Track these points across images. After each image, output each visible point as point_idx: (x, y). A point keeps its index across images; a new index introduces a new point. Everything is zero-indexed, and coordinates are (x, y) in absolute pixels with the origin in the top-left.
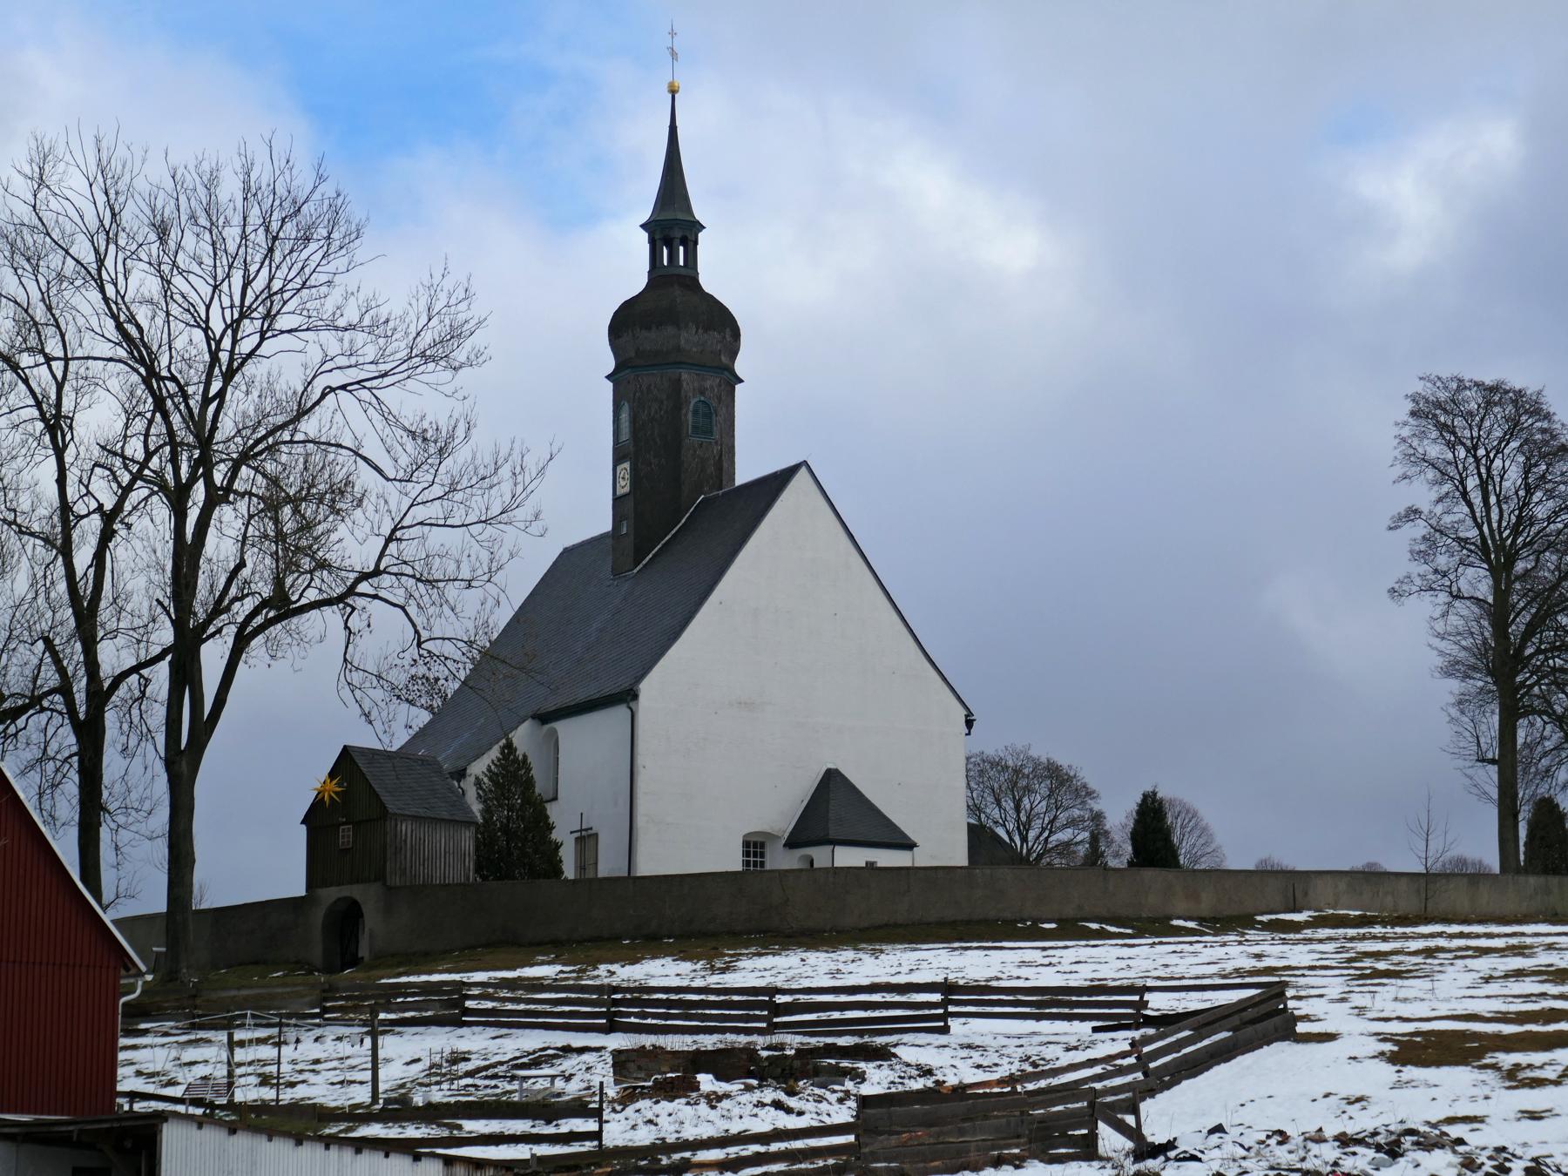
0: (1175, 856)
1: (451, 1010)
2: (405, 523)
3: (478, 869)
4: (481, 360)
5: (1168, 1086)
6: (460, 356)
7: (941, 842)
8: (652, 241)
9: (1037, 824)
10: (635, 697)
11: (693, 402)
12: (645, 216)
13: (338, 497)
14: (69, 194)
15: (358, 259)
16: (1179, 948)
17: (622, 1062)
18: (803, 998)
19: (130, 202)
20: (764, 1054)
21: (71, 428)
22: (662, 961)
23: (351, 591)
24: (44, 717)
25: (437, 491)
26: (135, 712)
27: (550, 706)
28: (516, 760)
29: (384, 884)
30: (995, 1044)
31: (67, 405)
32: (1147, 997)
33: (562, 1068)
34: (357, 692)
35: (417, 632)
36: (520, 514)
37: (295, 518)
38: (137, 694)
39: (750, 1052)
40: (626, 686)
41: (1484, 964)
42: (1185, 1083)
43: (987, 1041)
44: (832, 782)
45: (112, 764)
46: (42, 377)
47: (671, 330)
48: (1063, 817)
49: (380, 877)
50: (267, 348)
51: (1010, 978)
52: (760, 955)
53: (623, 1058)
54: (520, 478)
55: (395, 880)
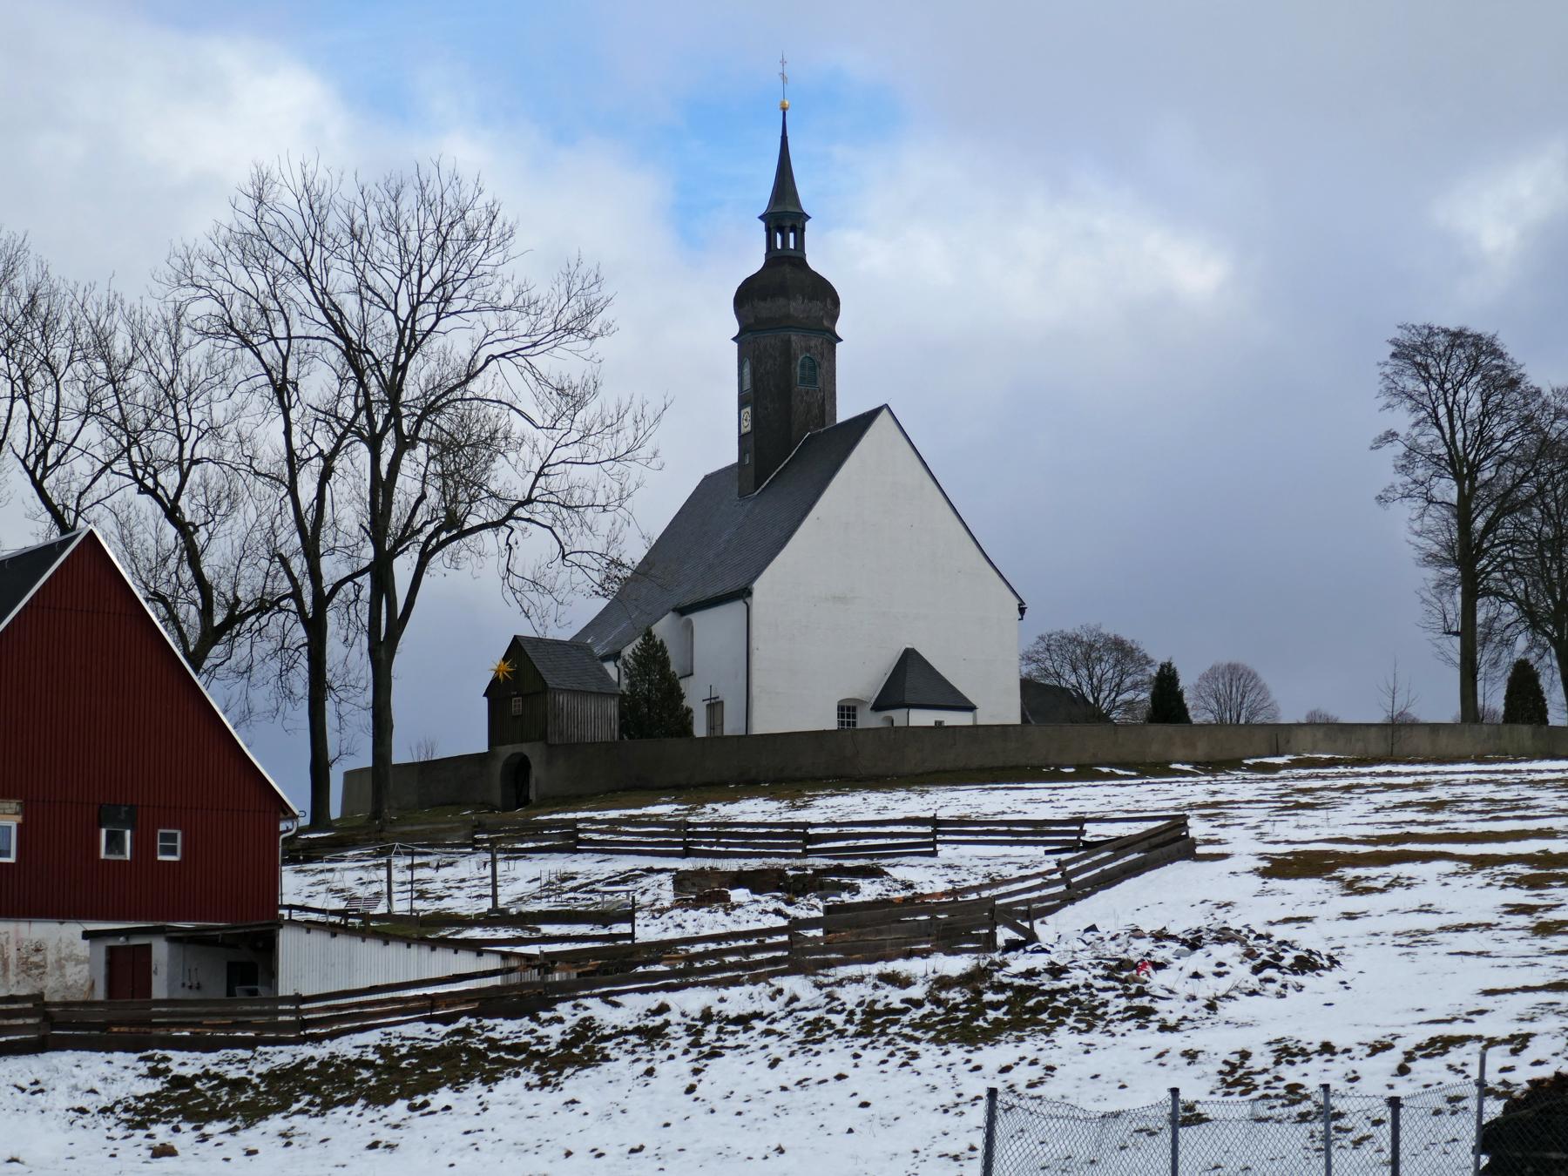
0: (1184, 711)
1: (571, 842)
2: (551, 461)
3: (622, 729)
5: (1086, 895)
6: (594, 328)
7: (999, 704)
8: (768, 230)
9: (1106, 687)
10: (750, 594)
12: (763, 209)
13: (490, 443)
14: (281, 208)
15: (512, 253)
16: (1155, 787)
17: (680, 880)
18: (846, 830)
19: (332, 213)
21: (296, 389)
23: (510, 516)
24: (282, 617)
25: (575, 436)
26: (352, 610)
27: (687, 601)
28: (655, 645)
31: (291, 375)
32: (1086, 826)
36: (642, 453)
37: (463, 458)
38: (352, 597)
39: (780, 873)
40: (743, 585)
41: (1381, 799)
42: (1100, 893)
43: (966, 863)
44: (910, 660)
45: (334, 648)
46: (269, 351)
47: (781, 301)
48: (1128, 681)
49: (543, 737)
50: (442, 326)
52: (832, 795)
55: (554, 739)
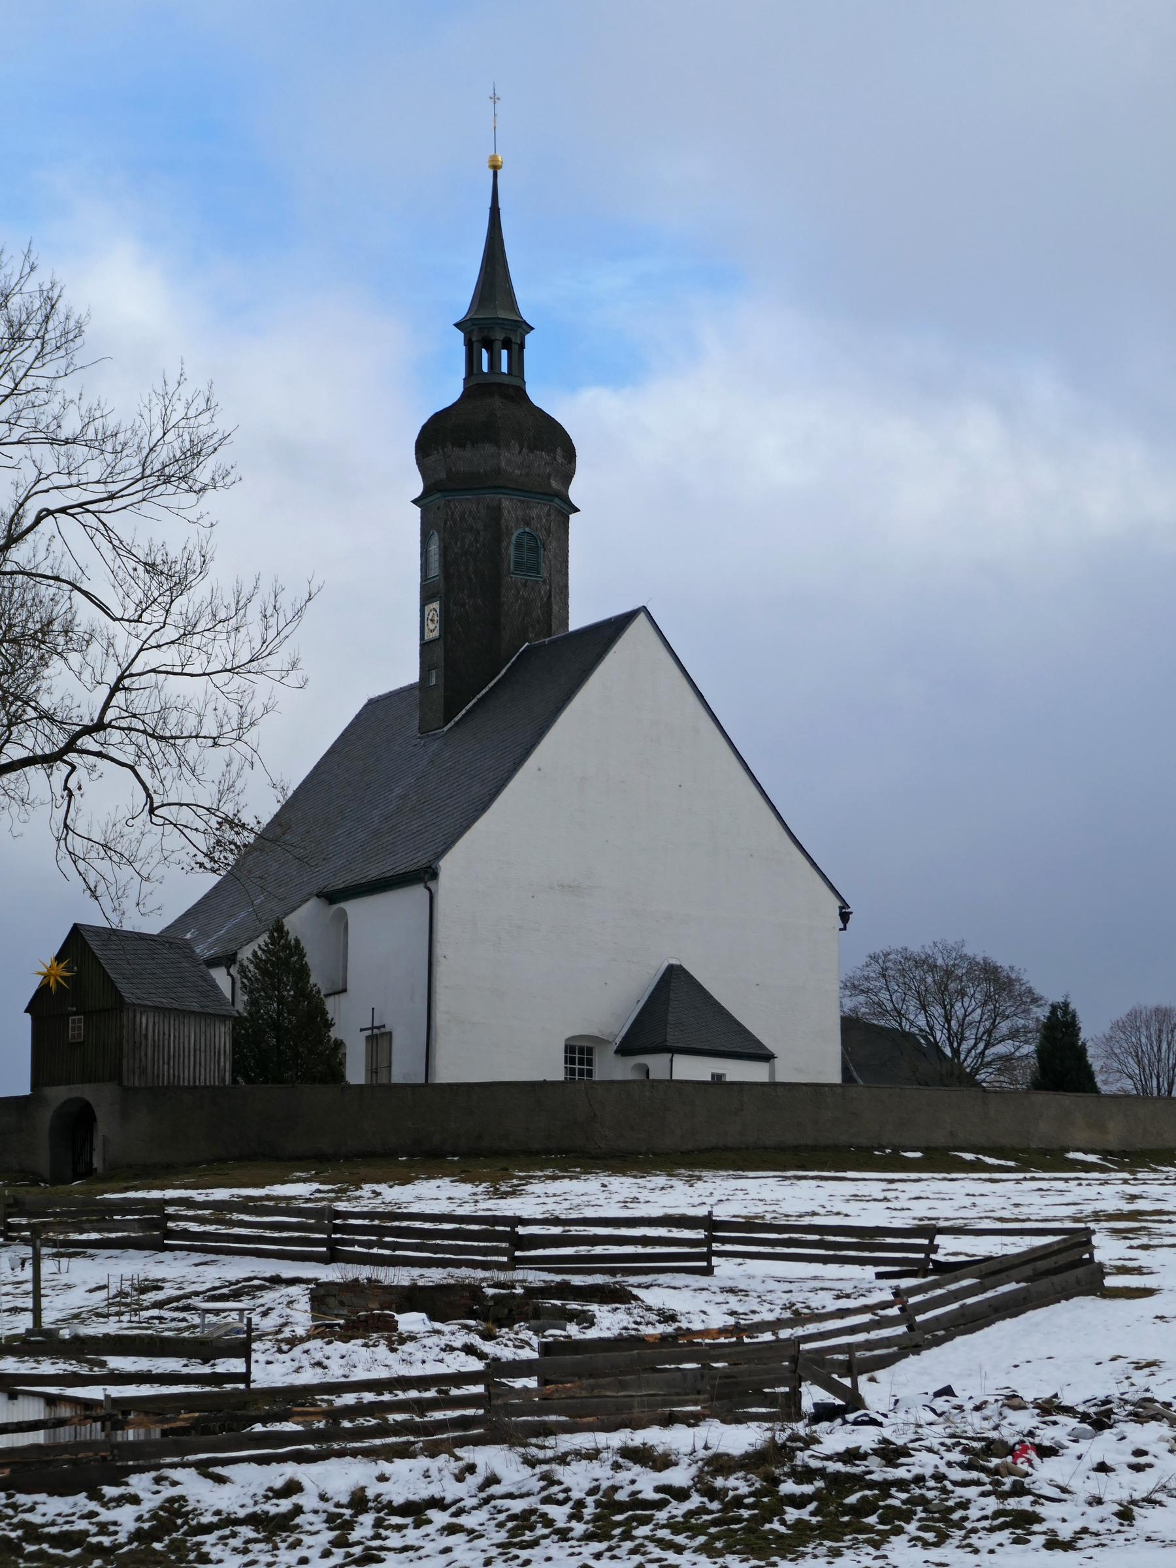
1: (156, 1234)
2: (135, 669)
3: (235, 1071)
4: (228, 480)
5: (938, 1342)
6: (203, 475)
7: (809, 1054)
8: (469, 343)
11: (516, 534)
12: (461, 313)
15: (78, 361)
18: (575, 1230)
20: (490, 1292)
22: (438, 1182)
23: (70, 747)
25: (171, 633)
27: (339, 884)
28: (287, 946)
29: (120, 1083)
30: (761, 1288)
32: (939, 1239)
33: (261, 1301)
34: (81, 864)
35: (149, 796)
36: (276, 662)
39: (475, 1291)
42: (959, 1340)
43: (755, 1286)
44: (675, 980)
47: (489, 449)
48: (1004, 1027)
49: (116, 1076)
51: (829, 1213)
52: (554, 1178)
53: (322, 1291)
54: (272, 621)
